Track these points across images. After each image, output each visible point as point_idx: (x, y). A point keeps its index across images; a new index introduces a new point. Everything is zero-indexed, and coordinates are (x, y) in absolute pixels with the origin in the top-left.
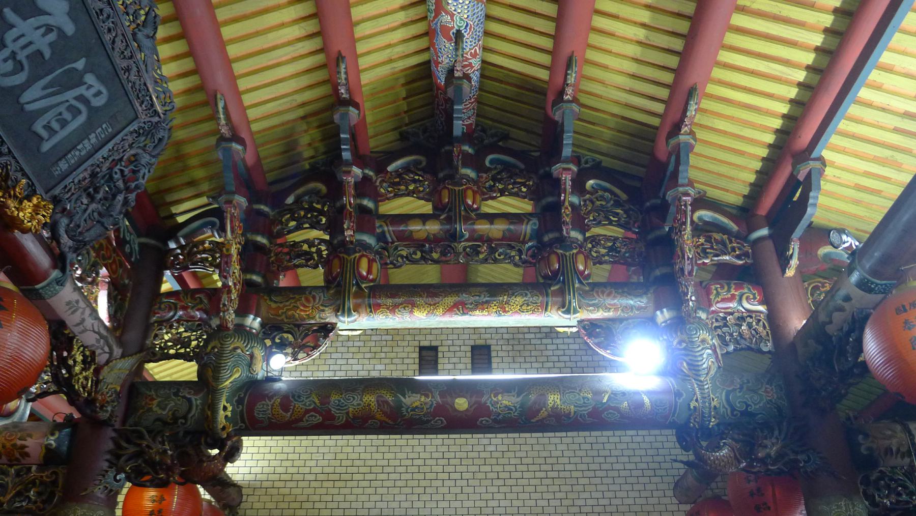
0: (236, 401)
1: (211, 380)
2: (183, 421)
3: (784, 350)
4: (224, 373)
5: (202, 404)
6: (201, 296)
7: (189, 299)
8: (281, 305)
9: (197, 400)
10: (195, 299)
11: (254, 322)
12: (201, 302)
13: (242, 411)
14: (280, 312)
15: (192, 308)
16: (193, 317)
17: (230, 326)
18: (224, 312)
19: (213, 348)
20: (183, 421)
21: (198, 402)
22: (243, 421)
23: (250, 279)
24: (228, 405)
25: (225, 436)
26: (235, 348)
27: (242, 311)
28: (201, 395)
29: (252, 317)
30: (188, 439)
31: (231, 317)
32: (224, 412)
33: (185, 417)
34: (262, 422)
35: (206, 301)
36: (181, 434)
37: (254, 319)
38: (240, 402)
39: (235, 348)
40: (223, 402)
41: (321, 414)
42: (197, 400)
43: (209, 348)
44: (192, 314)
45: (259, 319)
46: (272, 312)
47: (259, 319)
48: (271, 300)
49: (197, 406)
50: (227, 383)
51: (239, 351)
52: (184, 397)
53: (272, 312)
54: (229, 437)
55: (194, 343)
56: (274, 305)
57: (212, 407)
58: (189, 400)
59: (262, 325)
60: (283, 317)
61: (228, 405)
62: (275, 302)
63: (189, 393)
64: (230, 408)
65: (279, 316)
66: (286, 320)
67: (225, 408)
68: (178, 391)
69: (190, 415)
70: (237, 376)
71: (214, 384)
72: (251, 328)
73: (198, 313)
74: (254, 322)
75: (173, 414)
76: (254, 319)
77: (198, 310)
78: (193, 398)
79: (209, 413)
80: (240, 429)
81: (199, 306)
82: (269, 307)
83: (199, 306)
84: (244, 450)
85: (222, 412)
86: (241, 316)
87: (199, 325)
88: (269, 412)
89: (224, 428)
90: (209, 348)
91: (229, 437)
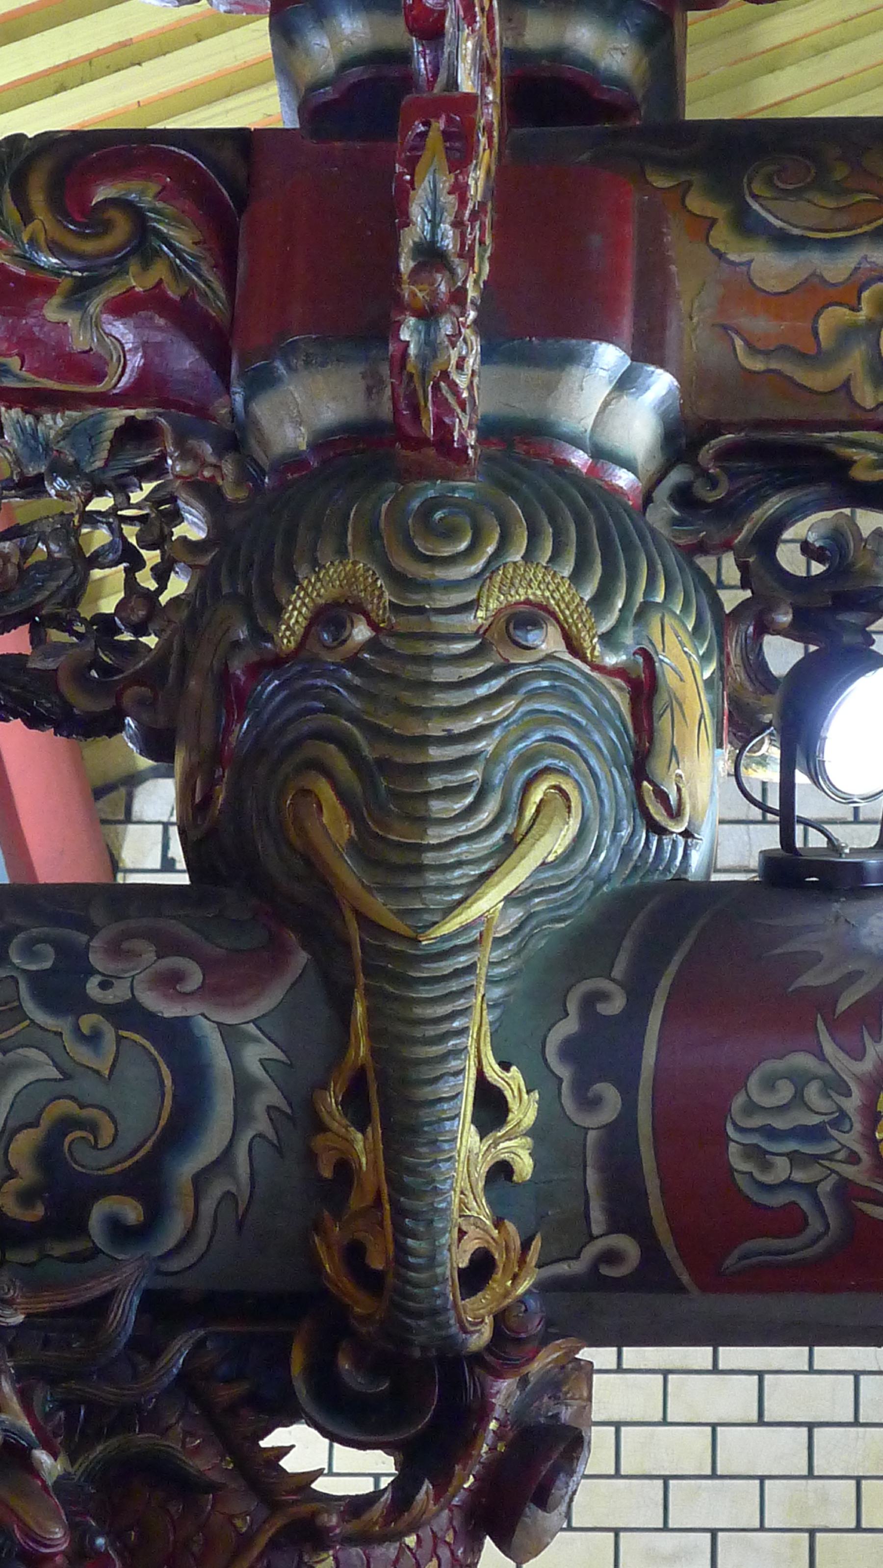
0: (570, 1050)
1: (348, 873)
2: (132, 1212)
3: (851, 458)
4: (453, 828)
5: (282, 1072)
6: (143, 192)
7: (43, 221)
8: (838, 268)
9: (245, 1043)
10: (94, 221)
11: (617, 406)
12: (143, 243)
13: (621, 1132)
14: (833, 318)
15: (79, 295)
16: (88, 367)
17: (465, 430)
18: (429, 315)
19: (332, 617)
20: (132, 1212)
21: (256, 1054)
22: (628, 1215)
23: (558, 54)
24: (511, 1082)
25: (480, 1338)
26: (528, 617)
27: (543, 315)
28: (269, 1001)
29: (609, 357)
30: (177, 1355)
31: (471, 375)
32: (483, 1148)
33: (146, 1181)
34: (790, 1221)
35: (184, 238)
36: (126, 1313)
37: (625, 383)
38: (601, 1053)
39: (528, 617)
40: (475, 1054)
41: (58, 1410)
42: (245, 1043)
43: (296, 616)
44: (80, 340)
45: (661, 383)
46: (762, 325)
47: (661, 383)
48: (746, 225)
49: (245, 1088)
50: (489, 900)
51: (547, 641)
52: (128, 1014)
53: (762, 325)
54: (509, 1342)
55: (108, 591)
56: (771, 267)
57: (391, 1097)
58: (176, 1040)
59: (681, 438)
60: (854, 363)
61: (511, 1082)
62: (783, 241)
63: (170, 982)
64: (524, 1110)
65: (816, 358)
66: (867, 396)
67: (491, 1108)
68: (74, 965)
69: (188, 1167)
70: (554, 841)
71: (381, 908)
72: (602, 454)
73: (121, 331)
74: (617, 406)
75: (48, 1155)
76: (625, 383)
77: (123, 307)
78: (208, 1023)
79: (362, 1146)
80: (594, 1281)
81: (136, 281)
82: (745, 291)
83: (136, 281)
84: (599, 1454)
85: (469, 1148)
86: (530, 359)
87: (134, 433)
88: (852, 1139)
89: (479, 1272)
90: (296, 616)
91: (509, 1342)
